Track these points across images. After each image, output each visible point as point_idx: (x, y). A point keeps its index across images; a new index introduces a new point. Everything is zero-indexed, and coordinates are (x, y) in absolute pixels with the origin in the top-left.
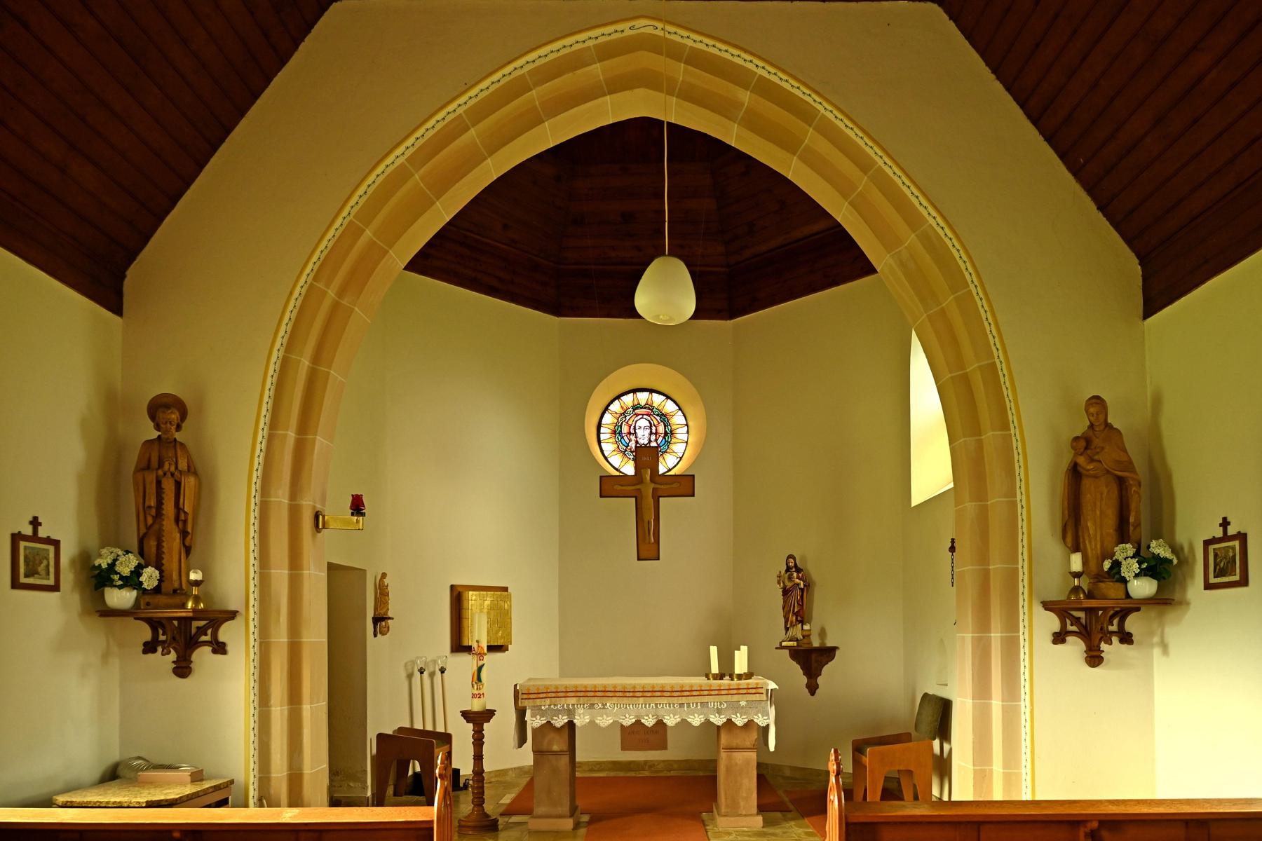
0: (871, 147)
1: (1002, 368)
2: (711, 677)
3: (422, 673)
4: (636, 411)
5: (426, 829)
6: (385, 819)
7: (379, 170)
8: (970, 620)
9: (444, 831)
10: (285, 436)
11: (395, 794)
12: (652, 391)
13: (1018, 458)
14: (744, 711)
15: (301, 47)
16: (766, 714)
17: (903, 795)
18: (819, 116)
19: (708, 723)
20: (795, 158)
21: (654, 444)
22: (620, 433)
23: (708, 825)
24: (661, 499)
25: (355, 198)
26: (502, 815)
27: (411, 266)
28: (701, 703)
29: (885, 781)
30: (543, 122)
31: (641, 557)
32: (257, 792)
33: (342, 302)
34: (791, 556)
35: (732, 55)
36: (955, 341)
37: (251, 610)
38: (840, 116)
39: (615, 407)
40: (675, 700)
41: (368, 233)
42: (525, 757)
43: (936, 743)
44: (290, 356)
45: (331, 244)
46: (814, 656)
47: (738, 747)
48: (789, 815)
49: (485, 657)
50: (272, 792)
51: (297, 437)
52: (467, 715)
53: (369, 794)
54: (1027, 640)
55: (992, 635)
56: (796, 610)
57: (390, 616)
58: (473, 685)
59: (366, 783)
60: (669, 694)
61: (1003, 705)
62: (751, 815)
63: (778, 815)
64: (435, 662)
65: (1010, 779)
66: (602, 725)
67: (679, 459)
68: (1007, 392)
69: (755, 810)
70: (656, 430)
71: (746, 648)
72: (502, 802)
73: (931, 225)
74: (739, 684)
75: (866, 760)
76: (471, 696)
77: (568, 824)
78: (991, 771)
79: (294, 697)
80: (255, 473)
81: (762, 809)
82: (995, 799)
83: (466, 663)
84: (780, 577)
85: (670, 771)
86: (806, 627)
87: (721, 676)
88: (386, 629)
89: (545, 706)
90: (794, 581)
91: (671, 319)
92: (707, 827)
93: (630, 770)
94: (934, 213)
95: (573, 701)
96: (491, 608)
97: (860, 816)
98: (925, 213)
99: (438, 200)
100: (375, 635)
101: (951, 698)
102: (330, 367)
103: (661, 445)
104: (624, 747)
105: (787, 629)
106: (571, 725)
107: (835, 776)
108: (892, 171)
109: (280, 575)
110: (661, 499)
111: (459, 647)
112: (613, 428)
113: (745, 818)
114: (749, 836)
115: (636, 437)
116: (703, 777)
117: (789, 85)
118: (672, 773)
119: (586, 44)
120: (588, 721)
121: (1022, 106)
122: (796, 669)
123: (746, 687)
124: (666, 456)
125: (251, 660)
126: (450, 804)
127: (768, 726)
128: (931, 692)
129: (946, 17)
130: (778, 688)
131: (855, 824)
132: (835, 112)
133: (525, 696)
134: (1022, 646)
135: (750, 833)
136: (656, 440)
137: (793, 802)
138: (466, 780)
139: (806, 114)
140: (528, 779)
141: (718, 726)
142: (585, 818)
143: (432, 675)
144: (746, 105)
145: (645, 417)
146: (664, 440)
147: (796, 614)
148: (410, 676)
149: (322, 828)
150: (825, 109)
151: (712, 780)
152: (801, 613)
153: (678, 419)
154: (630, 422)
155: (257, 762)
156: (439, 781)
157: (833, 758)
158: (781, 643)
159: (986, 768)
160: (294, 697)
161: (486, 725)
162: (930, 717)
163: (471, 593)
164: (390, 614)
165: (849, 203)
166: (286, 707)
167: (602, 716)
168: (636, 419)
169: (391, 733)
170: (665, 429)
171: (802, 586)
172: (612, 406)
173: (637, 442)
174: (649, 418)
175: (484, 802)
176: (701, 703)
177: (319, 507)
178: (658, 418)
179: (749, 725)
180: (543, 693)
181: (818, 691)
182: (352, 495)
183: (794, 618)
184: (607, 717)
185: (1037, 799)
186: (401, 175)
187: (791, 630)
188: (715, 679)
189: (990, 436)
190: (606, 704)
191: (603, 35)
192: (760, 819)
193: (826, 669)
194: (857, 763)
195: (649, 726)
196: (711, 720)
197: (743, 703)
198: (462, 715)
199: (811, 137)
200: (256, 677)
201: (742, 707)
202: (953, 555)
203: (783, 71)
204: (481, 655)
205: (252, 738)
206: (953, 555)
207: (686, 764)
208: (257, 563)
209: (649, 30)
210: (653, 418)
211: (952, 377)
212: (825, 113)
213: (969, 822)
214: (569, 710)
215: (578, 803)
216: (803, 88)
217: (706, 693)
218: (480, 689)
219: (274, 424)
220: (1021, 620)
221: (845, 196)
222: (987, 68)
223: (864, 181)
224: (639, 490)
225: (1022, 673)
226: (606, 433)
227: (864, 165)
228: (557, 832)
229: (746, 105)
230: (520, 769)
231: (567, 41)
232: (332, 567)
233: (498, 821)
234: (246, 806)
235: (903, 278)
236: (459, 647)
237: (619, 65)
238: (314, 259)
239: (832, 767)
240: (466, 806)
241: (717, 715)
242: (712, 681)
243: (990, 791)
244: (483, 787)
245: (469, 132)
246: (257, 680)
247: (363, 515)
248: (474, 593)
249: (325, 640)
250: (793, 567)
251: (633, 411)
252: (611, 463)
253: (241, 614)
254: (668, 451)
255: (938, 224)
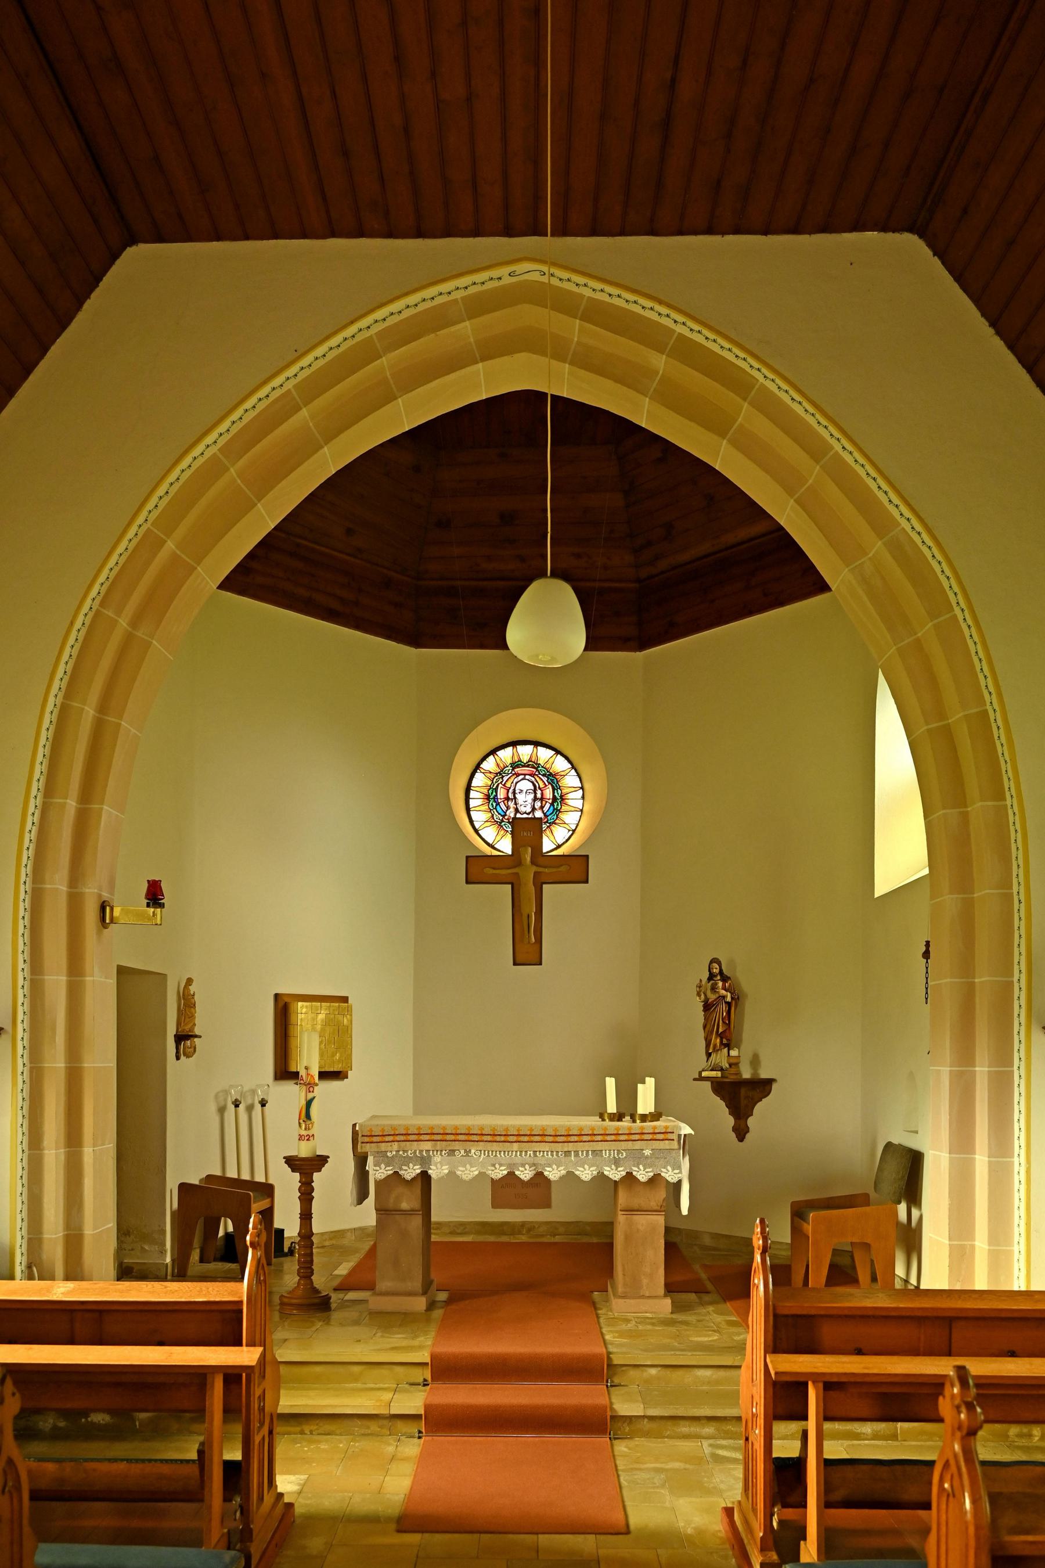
0: (826, 427)
1: (995, 717)
2: (606, 1118)
3: (237, 1106)
4: (516, 770)
5: (234, 1311)
6: (181, 1297)
7: (184, 464)
8: (948, 1052)
9: (255, 1315)
10: (63, 806)
11: (202, 1261)
12: (537, 744)
13: (1015, 836)
14: (649, 1161)
15: (87, 306)
16: (677, 1166)
17: (856, 1274)
18: (757, 387)
19: (601, 1177)
20: (725, 442)
21: (539, 814)
22: (495, 798)
23: (601, 1309)
24: (544, 886)
25: (154, 500)
26: (335, 1289)
27: (227, 585)
28: (593, 1151)
29: (833, 1255)
30: (396, 398)
31: (518, 961)
32: (25, 1258)
33: (136, 633)
34: (714, 960)
35: (643, 308)
36: (933, 682)
37: (20, 1027)
38: (785, 387)
39: (490, 764)
40: (558, 1147)
41: (170, 545)
42: (367, 1215)
43: (902, 1208)
44: (72, 703)
45: (124, 558)
46: (743, 1091)
47: (640, 1209)
48: (706, 1298)
49: (316, 1088)
50: (44, 1257)
51: (79, 806)
52: (292, 1162)
53: (168, 1260)
54: (1023, 1076)
55: (977, 1069)
56: (721, 1030)
57: (197, 1034)
58: (300, 1123)
59: (165, 1245)
60: (551, 1139)
61: (990, 1162)
62: (656, 1297)
63: (692, 1296)
64: (254, 1092)
65: (999, 1260)
66: (464, 1177)
67: (571, 832)
68: (1002, 749)
69: (661, 1291)
70: (542, 794)
71: (653, 1079)
72: (336, 1272)
73: (903, 529)
74: (642, 1128)
75: (809, 1228)
76: (298, 1137)
77: (420, 1303)
78: (973, 1247)
79: (73, 1138)
80: (25, 852)
81: (670, 1289)
82: (977, 1288)
83: (291, 1094)
84: (700, 987)
85: (555, 1235)
86: (734, 1053)
87: (619, 1117)
88: (192, 1050)
89: (391, 1152)
90: (718, 992)
91: (553, 660)
92: (599, 1312)
93: (504, 1234)
94: (907, 513)
95: (428, 1146)
96: (327, 1023)
97: (791, 1306)
98: (895, 513)
99: (259, 501)
100: (178, 1058)
101: (922, 1150)
102: (121, 717)
103: (548, 813)
104: (495, 1204)
105: (709, 1055)
106: (425, 1178)
107: (761, 1254)
108: (852, 458)
109: (56, 982)
110: (544, 886)
111: (285, 1072)
112: (485, 791)
113: (650, 1301)
114: (653, 1324)
115: (516, 804)
116: (597, 1244)
117: (719, 346)
118: (557, 1239)
119: (452, 297)
120: (446, 1171)
121: (1030, 370)
122: (720, 1106)
123: (651, 1131)
124: (555, 828)
125: (20, 1090)
126: (265, 1280)
127: (679, 1182)
128: (896, 1141)
129: (929, 252)
130: (693, 1133)
131: (786, 1316)
132: (778, 381)
133: (366, 1139)
134: (1016, 1085)
135: (653, 1321)
136: (542, 807)
137: (714, 1280)
138: (292, 1243)
139: (741, 385)
140: (372, 1243)
141: (615, 1181)
142: (442, 1296)
143: (250, 1109)
144: (661, 372)
145: (527, 777)
146: (552, 808)
147: (721, 1036)
148: (222, 1110)
149: (101, 1307)
150: (765, 377)
151: (608, 1248)
152: (727, 1034)
153: (571, 781)
154: (508, 785)
155: (26, 1219)
156: (250, 1251)
157: (759, 1230)
158: (700, 1073)
159: (966, 1243)
160: (73, 1138)
161: (316, 1175)
162: (895, 1171)
163: (300, 1004)
164: (197, 1031)
165: (795, 500)
166: (62, 1150)
167: (465, 1166)
168: (516, 780)
169: (197, 1183)
170: (554, 793)
171: (729, 999)
172: (485, 763)
173: (517, 811)
174: (533, 779)
175: (312, 1273)
176: (593, 1151)
177: (106, 895)
178: (545, 779)
179: (655, 1180)
180: (389, 1135)
181: (748, 1136)
182: (148, 881)
183: (718, 1040)
184: (471, 1167)
185: (1033, 1288)
186: (213, 470)
187: (713, 1056)
188: (611, 1120)
189: (978, 807)
190: (470, 1151)
191: (475, 283)
192: (668, 1301)
193: (759, 1108)
194: (796, 1231)
195: (526, 1179)
196: (606, 1173)
197: (647, 1152)
198: (286, 1162)
199: (746, 415)
200: (26, 1111)
201: (647, 1157)
202: (927, 962)
203: (710, 328)
204: (310, 1086)
205: (19, 1189)
206: (927, 962)
207: (575, 1227)
208: (27, 967)
209: (535, 277)
210: (538, 779)
211: (928, 730)
212: (765, 383)
213: (937, 1318)
214: (422, 1158)
215: (433, 1275)
216: (736, 350)
217: (599, 1138)
218: (309, 1129)
219: (49, 791)
220: (1016, 1050)
221: (790, 491)
222: (983, 320)
223: (816, 471)
224: (517, 874)
225: (1016, 1120)
226: (476, 799)
227: (817, 450)
228: (405, 1314)
229: (661, 372)
230: (362, 1229)
231: (411, 299)
232: (122, 971)
233: (330, 1298)
234: (12, 1278)
235: (865, 598)
236: (285, 1072)
237: (498, 322)
238: (102, 578)
239: (758, 1242)
240: (290, 1278)
241: (613, 1166)
242: (607, 1123)
243: (971, 1275)
244: (311, 1254)
245: (301, 412)
246: (27, 1116)
247: (162, 906)
248: (305, 1004)
249: (113, 1064)
250: (718, 974)
251: (513, 770)
252: (483, 837)
253: (7, 1032)
254: (557, 821)
255: (913, 528)
